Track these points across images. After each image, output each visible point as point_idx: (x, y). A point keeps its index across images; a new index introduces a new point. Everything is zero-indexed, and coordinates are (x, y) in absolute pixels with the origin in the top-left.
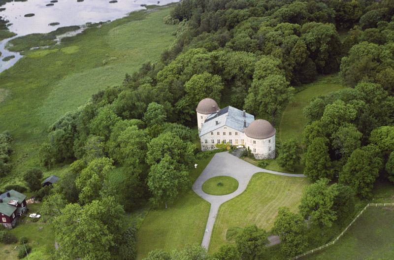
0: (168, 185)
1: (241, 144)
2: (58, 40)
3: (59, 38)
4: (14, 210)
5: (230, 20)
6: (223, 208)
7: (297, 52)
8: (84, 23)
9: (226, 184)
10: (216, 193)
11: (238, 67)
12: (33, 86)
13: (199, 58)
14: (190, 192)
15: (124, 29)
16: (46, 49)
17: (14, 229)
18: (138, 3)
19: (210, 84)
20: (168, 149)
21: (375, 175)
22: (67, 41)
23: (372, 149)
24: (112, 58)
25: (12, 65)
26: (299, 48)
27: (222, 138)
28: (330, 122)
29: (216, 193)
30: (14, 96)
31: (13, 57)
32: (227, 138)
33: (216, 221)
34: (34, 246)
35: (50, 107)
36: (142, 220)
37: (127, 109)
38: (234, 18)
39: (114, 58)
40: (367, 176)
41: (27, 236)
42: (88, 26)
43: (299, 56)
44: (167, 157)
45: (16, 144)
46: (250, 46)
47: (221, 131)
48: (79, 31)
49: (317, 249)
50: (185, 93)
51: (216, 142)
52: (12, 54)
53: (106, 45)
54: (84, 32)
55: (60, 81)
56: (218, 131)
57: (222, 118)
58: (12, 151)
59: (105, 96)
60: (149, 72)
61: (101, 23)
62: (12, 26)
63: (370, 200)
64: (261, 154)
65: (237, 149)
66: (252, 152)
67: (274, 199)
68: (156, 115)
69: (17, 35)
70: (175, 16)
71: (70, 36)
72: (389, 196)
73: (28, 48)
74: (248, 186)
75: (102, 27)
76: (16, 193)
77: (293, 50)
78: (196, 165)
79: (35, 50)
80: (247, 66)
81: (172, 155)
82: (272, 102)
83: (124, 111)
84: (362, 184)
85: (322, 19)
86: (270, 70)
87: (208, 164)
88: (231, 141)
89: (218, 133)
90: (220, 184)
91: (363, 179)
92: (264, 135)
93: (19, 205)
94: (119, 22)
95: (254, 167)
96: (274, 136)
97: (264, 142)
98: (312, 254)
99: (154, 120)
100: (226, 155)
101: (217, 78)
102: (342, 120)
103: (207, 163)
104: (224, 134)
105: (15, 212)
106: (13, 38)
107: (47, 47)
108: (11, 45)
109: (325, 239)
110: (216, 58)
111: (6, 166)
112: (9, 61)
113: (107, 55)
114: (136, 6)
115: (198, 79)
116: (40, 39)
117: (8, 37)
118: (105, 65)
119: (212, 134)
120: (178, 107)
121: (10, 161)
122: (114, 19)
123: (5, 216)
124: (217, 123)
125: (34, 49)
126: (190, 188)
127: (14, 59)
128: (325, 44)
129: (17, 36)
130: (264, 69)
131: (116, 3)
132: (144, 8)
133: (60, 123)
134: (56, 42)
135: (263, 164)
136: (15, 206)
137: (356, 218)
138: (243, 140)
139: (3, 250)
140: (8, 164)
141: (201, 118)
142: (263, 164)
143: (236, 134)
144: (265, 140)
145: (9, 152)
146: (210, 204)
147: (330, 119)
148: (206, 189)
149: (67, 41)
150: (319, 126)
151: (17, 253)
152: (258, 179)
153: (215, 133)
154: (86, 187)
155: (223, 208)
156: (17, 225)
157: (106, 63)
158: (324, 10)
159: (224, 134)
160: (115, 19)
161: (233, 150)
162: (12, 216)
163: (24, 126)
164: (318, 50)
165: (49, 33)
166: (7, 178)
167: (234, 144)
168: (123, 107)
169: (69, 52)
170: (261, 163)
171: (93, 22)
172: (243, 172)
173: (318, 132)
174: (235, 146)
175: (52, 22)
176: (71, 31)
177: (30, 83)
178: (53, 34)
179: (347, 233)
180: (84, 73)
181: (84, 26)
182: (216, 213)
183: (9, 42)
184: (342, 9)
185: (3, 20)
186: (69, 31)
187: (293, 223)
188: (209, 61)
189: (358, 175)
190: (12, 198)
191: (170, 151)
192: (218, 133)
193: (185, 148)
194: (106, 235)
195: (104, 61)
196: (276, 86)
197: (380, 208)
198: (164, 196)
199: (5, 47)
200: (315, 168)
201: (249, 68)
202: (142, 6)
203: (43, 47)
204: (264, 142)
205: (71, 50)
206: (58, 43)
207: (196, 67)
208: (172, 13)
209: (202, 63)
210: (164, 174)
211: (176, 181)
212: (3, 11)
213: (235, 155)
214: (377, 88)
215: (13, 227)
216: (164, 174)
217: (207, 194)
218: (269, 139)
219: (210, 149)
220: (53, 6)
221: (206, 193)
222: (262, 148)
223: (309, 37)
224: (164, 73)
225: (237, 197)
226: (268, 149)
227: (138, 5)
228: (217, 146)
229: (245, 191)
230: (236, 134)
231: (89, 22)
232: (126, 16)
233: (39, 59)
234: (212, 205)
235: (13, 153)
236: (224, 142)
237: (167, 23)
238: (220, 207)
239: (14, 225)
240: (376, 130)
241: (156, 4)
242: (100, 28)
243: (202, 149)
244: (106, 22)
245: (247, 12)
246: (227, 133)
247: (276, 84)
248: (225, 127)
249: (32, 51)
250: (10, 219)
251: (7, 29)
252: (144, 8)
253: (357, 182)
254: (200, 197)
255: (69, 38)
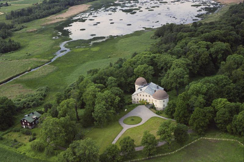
3: (92, 42)
4: (34, 120)
7: (203, 58)
8: (108, 36)
10: (129, 123)
11: (164, 63)
15: (128, 40)
16: (84, 48)
17: (33, 130)
19: (146, 71)
22: (95, 45)
23: (210, 108)
27: (142, 98)
28: (192, 93)
29: (129, 123)
30: (58, 70)
31: (66, 51)
32: (145, 98)
33: (121, 136)
35: (73, 77)
38: (180, 37)
39: (115, 55)
40: (201, 123)
41: (36, 133)
44: (104, 102)
45: (50, 93)
46: (179, 53)
47: (142, 94)
48: (104, 40)
49: (163, 154)
50: (134, 74)
51: (139, 100)
52: (66, 49)
53: (114, 48)
56: (141, 94)
57: (144, 88)
58: (46, 96)
63: (204, 135)
66: (155, 106)
67: (155, 129)
69: (72, 39)
70: (156, 34)
71: (98, 42)
72: (215, 135)
73: (75, 47)
78: (126, 110)
79: (77, 48)
80: (169, 62)
81: (107, 102)
82: (175, 82)
84: (198, 126)
85: (231, 40)
86: (179, 65)
88: (147, 100)
89: (140, 95)
90: (133, 120)
91: (199, 124)
92: (162, 97)
94: (127, 36)
95: (154, 113)
96: (168, 98)
98: (160, 157)
99: (110, 85)
100: (144, 107)
103: (133, 109)
104: (143, 96)
105: (34, 121)
106: (70, 41)
108: (67, 45)
112: (63, 53)
114: (140, 28)
118: (109, 58)
119: (138, 95)
120: (128, 81)
122: (125, 34)
123: (29, 122)
125: (77, 48)
126: (118, 120)
128: (220, 54)
129: (72, 40)
132: (144, 29)
133: (73, 84)
134: (90, 45)
135: (159, 113)
136: (34, 118)
138: (151, 100)
139: (24, 138)
142: (159, 113)
143: (149, 96)
144: (161, 100)
145: (45, 96)
146: (123, 128)
148: (125, 122)
149: (95, 45)
150: (185, 95)
151: (29, 139)
152: (152, 120)
156: (34, 127)
157: (110, 57)
159: (143, 96)
161: (147, 104)
162: (32, 123)
163: (57, 85)
166: (39, 107)
167: (148, 101)
168: (97, 78)
169: (94, 50)
171: (113, 35)
174: (149, 103)
176: (99, 39)
177: (68, 64)
178: (90, 40)
179: (183, 150)
180: (97, 61)
181: (107, 37)
182: (124, 132)
183: (67, 43)
185: (69, 32)
187: (148, 138)
189: (196, 121)
190: (34, 115)
192: (140, 95)
193: (114, 99)
194: (62, 133)
195: (109, 56)
199: (64, 45)
200: (179, 116)
201: (170, 64)
202: (143, 28)
203: (82, 47)
205: (96, 49)
206: (91, 45)
208: (155, 33)
209: (146, 59)
212: (70, 27)
214: (225, 78)
215: (32, 128)
218: (164, 100)
219: (137, 103)
221: (124, 123)
222: (160, 104)
224: (126, 63)
226: (163, 106)
228: (140, 102)
230: (149, 96)
232: (132, 33)
236: (143, 100)
237: (151, 38)
239: (33, 127)
240: (215, 100)
241: (152, 27)
243: (133, 103)
246: (145, 96)
248: (144, 92)
250: (31, 124)
252: (144, 29)
255: (98, 43)
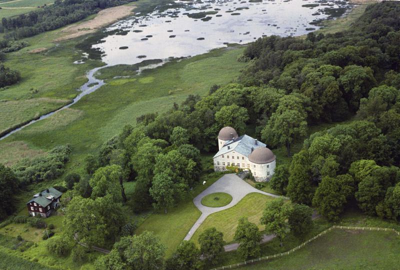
0: (164, 192)
1: (247, 168)
2: (140, 71)
4: (49, 203)
5: (285, 60)
6: (210, 217)
7: (329, 92)
8: (167, 57)
9: (222, 199)
11: (264, 101)
12: (104, 109)
13: (233, 92)
14: (190, 203)
15: (200, 64)
16: (127, 78)
18: (238, 38)
20: (171, 164)
21: (342, 201)
22: (146, 73)
24: (178, 89)
25: (94, 91)
26: (332, 88)
27: (231, 161)
30: (86, 116)
32: (236, 162)
33: (200, 227)
34: (58, 232)
36: (143, 220)
37: (157, 131)
41: (54, 225)
42: (170, 60)
43: (330, 96)
44: (168, 170)
46: (289, 85)
48: (160, 64)
50: (215, 122)
51: (226, 164)
52: (97, 81)
53: (178, 78)
54: (164, 66)
55: (128, 106)
57: (234, 145)
59: (145, 119)
60: (378, 123)
61: (182, 58)
62: (106, 56)
64: (260, 177)
65: (243, 172)
66: (253, 175)
68: (179, 138)
69: (107, 64)
70: (246, 55)
73: (112, 77)
74: (239, 202)
75: (182, 61)
76: (55, 190)
77: (326, 90)
78: (204, 182)
81: (174, 169)
83: (155, 132)
84: (329, 208)
87: (215, 182)
88: (238, 165)
89: (228, 157)
90: (217, 199)
91: (330, 203)
92: (264, 160)
93: (55, 200)
94: (198, 58)
97: (262, 167)
98: (267, 260)
99: (177, 141)
100: (234, 177)
101: (244, 110)
102: (328, 151)
104: (233, 157)
105: (50, 205)
107: (128, 77)
108: (99, 74)
109: (283, 249)
110: (249, 93)
111: (58, 171)
112: (92, 87)
113: (175, 86)
114: (220, 43)
115: (225, 111)
116: (125, 70)
117: (100, 66)
119: (223, 157)
121: (64, 168)
123: (41, 207)
124: (229, 148)
127: (97, 85)
129: (106, 66)
130: (285, 105)
131: (203, 40)
132: (226, 46)
133: (113, 140)
134: (137, 73)
135: (260, 186)
136: (51, 200)
137: (317, 236)
138: (246, 164)
139: (34, 233)
140: (62, 170)
141: (221, 143)
142: (260, 186)
143: (243, 158)
144: (263, 165)
147: (315, 149)
149: (146, 73)
150: (304, 155)
153: (225, 156)
154: (96, 187)
155: (210, 217)
156: (51, 215)
157: (172, 94)
158: (377, 55)
159: (233, 157)
160: (195, 55)
161: (240, 172)
162: (47, 207)
163: (86, 141)
164: (351, 92)
165: (134, 65)
166: (57, 181)
167: (241, 167)
169: (145, 82)
170: (257, 185)
172: (238, 189)
173: (302, 159)
174: (242, 170)
175: (140, 55)
177: (102, 106)
178: (138, 65)
180: (150, 101)
181: (166, 60)
183: (99, 70)
184: (396, 54)
186: (151, 63)
187: (247, 229)
188: (240, 95)
189: (325, 198)
190: (50, 194)
191: (173, 165)
192: (228, 157)
195: (170, 92)
196: (289, 120)
197: (344, 230)
198: (162, 201)
199: (94, 75)
200: (295, 191)
202: (225, 43)
204: (262, 167)
206: (139, 74)
207: (229, 99)
208: (245, 51)
210: (161, 183)
211: (172, 190)
212: (103, 43)
213: (240, 177)
214: (369, 126)
215: (47, 217)
216: (161, 183)
217: (202, 206)
218: (267, 164)
220: (147, 41)
221: (204, 205)
222: (261, 172)
223: (343, 79)
225: (226, 210)
227: (221, 43)
228: (228, 168)
229: (235, 206)
230: (243, 158)
231: (172, 56)
232: (207, 52)
233: (117, 86)
234: (202, 215)
235: (68, 162)
236: (233, 165)
237: (239, 61)
238: (208, 217)
239: (48, 215)
241: (238, 43)
242: (181, 62)
243: (215, 170)
244: (186, 57)
245: (302, 53)
246: (235, 158)
247: (289, 118)
248: (233, 151)
249: (114, 79)
250: (45, 210)
251: (101, 59)
252: (226, 46)
253: (324, 205)
254: (196, 207)
255: (150, 69)
